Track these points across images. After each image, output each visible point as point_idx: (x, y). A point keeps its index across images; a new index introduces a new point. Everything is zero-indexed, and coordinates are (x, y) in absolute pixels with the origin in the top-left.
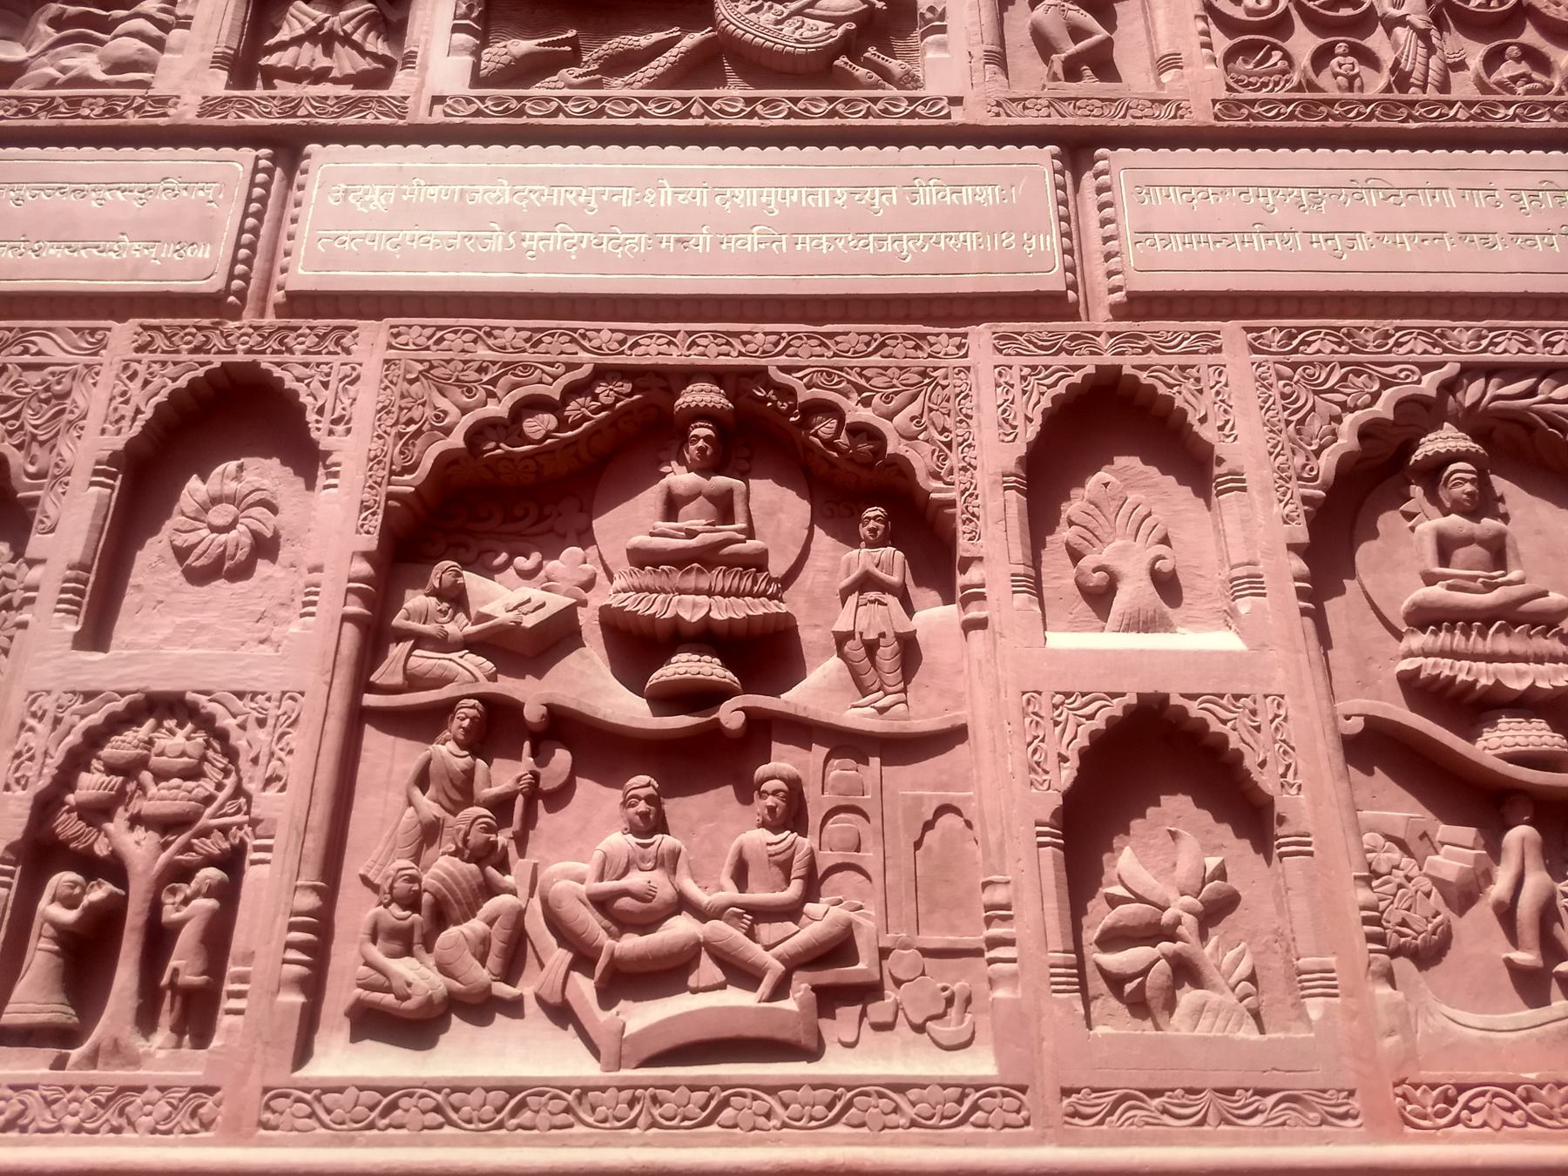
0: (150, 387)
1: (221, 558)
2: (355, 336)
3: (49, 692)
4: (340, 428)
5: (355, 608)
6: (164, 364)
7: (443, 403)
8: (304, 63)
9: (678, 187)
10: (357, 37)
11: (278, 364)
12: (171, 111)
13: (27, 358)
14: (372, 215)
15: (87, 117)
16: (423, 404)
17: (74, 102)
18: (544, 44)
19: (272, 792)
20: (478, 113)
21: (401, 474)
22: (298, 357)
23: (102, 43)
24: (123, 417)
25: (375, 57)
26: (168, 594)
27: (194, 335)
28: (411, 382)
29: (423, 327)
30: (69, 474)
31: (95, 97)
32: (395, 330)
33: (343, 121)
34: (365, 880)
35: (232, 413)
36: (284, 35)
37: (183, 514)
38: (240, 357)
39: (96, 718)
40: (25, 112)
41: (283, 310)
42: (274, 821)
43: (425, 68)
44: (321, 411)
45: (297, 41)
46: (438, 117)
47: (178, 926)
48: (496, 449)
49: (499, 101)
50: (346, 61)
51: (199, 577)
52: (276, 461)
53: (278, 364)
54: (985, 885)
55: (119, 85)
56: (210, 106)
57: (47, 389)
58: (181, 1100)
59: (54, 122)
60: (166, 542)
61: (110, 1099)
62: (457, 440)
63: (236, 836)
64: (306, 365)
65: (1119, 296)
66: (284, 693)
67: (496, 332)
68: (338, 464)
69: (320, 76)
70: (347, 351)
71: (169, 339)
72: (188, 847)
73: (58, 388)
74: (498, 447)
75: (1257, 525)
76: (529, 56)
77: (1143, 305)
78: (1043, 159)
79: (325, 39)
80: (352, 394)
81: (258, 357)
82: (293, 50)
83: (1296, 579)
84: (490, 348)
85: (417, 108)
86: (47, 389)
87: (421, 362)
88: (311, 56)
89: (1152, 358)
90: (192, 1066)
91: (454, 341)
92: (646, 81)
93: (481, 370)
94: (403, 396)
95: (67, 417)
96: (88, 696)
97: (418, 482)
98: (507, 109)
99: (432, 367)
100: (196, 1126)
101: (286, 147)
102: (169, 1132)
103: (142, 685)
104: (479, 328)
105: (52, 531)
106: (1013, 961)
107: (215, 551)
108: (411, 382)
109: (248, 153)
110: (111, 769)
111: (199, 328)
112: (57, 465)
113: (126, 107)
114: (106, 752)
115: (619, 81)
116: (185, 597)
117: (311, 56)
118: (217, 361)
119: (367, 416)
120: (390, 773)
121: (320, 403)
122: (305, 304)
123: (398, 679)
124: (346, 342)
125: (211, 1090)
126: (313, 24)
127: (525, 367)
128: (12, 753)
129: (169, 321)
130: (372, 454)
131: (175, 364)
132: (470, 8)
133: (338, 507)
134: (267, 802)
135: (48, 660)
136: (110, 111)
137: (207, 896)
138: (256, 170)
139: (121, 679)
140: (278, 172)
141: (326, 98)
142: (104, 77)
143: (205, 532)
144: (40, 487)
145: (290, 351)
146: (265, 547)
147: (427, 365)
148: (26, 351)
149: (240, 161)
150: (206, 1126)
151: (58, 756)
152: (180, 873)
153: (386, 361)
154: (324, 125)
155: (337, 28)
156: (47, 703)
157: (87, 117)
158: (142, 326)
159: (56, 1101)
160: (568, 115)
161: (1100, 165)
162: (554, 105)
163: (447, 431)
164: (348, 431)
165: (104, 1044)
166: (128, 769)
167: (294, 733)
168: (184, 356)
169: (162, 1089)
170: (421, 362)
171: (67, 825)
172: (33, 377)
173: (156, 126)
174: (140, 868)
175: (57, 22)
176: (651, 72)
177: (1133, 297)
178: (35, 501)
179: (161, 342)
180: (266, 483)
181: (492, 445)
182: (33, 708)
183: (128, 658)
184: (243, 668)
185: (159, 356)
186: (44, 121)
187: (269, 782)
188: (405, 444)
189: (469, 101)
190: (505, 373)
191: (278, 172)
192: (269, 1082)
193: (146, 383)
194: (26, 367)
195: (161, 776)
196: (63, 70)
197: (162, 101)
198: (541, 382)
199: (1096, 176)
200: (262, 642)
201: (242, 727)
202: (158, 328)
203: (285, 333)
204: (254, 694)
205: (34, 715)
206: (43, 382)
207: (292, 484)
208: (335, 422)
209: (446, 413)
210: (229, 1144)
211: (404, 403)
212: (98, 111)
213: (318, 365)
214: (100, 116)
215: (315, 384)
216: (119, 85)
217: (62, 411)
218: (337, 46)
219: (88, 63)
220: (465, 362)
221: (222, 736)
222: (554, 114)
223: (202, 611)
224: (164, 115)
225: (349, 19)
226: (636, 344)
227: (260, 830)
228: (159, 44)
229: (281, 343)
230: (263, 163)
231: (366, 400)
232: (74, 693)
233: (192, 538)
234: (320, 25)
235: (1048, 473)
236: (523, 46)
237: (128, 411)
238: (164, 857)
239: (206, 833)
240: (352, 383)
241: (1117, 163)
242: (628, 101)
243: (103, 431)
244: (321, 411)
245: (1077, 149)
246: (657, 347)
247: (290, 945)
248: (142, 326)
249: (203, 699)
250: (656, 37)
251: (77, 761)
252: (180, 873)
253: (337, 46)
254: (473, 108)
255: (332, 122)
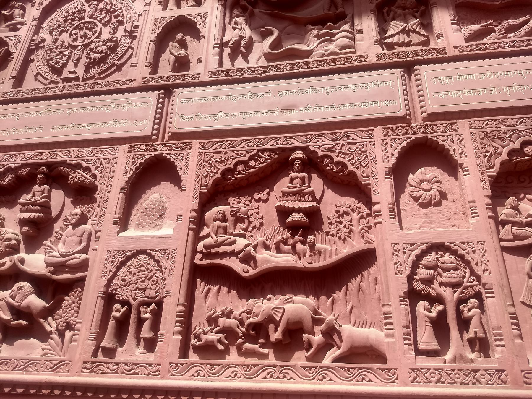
0: (393, 147)
1: (431, 200)
2: (457, 126)
3: (398, 244)
4: (463, 155)
5: (192, 226)
6: (395, 139)
7: (496, 145)
8: (401, 40)
9: (495, 73)
10: (417, 30)
11: (434, 137)
12: (367, 60)
13: (349, 141)
14: (191, 110)
15: (340, 65)
16: (489, 146)
17: (334, 60)
18: (483, 26)
19: (486, 274)
20: (471, 50)
21: (489, 169)
22: (440, 134)
23: (334, 41)
24: (388, 157)
25: (424, 35)
26: (416, 212)
27: (402, 130)
28: (482, 139)
29: (479, 121)
30: (377, 176)
31: (340, 58)
32: (470, 123)
33: (426, 57)
34: (523, 303)
35: (155, 171)
36: (389, 34)
37: (411, 186)
38: (420, 135)
39: (418, 251)
40: (319, 65)
41: (171, 138)
42: (492, 284)
43: (447, 38)
44: (454, 150)
45: (398, 34)
46: (456, 53)
47: (471, 318)
48: (517, 159)
49: (477, 46)
50: (415, 38)
51: (424, 206)
52: (435, 168)
53: (434, 137)
54: (383, 305)
55: (346, 53)
56: (379, 57)
57: (360, 150)
58: (493, 374)
59: (330, 67)
60: (408, 195)
61: (469, 373)
62: (219, 175)
63: (477, 289)
64: (444, 136)
65: (425, 115)
66: (478, 242)
67: (505, 120)
68: (467, 167)
69: (408, 44)
70: (456, 131)
71: (394, 131)
72: (462, 293)
73: (363, 149)
74: (517, 158)
75: (472, 185)
76: (479, 30)
77: (434, 117)
78: (399, 71)
79: (407, 32)
80: (463, 144)
81: (427, 135)
82: (396, 37)
83: (486, 205)
84: (505, 126)
85: (450, 51)
86: (360, 150)
87: (483, 132)
88: (403, 38)
89: (173, 152)
90: (150, 357)
91: (493, 124)
92: (522, 34)
93: (505, 133)
94: (481, 144)
95: (369, 158)
96: (412, 244)
97: (497, 171)
98: (481, 48)
99: (488, 133)
100: (500, 382)
101: (168, 90)
102: (493, 384)
103: (429, 241)
104: (499, 120)
105: (378, 193)
106: (392, 329)
107: (428, 198)
108: (482, 139)
109: (156, 92)
110: (427, 268)
111: (403, 127)
112: (372, 173)
113: (352, 60)
114: (423, 262)
115: (511, 35)
116: (422, 212)
117: (403, 38)
118: (413, 137)
119: (194, 167)
120: (517, 268)
121: (453, 148)
122: (176, 136)
123: (511, 237)
124: (455, 127)
125: (503, 371)
126: (402, 28)
127: (520, 131)
128: (393, 263)
129: (392, 126)
130: (478, 163)
131: (399, 139)
132: (455, 17)
133: (473, 181)
134: (485, 277)
135: (394, 233)
136: (347, 62)
137: (476, 308)
138: (159, 98)
139: (421, 239)
140: (166, 99)
141: (417, 50)
142: (340, 51)
143: (422, 191)
144: (369, 180)
145: (437, 132)
146: (443, 195)
147: (486, 133)
148: (348, 139)
149: (153, 97)
150: (505, 383)
151: (410, 264)
152: (462, 301)
153: (471, 133)
154: (420, 59)
155: (410, 28)
156: (399, 247)
157: (340, 65)
158: (383, 128)
159: (451, 374)
160: (502, 48)
161: (417, 72)
162: (497, 45)
163: (500, 154)
164: (466, 156)
165: (457, 356)
166: (434, 267)
167: (487, 255)
168: (401, 137)
169: (485, 371)
170: (483, 132)
171: (418, 286)
172: (354, 147)
173: (333, 68)
174: (449, 299)
175: (318, 37)
176: (524, 31)
177: (430, 115)
178: (369, 184)
179: (391, 133)
180: (436, 175)
181: (515, 158)
182: (395, 248)
183: (421, 232)
184: (461, 234)
185: (392, 137)
186: (326, 67)
187: (485, 270)
188: (488, 159)
189: (467, 47)
190: (513, 134)
191: (166, 99)
192: (523, 369)
193: (392, 146)
194: (350, 144)
195: (445, 270)
196: (326, 51)
197: (363, 57)
198: (527, 136)
199: (416, 75)
200: (453, 226)
201: (468, 253)
202: (389, 128)
203: (433, 126)
204: (468, 243)
205: (396, 251)
206: (357, 148)
207: (443, 175)
208: (461, 153)
209: (498, 148)
210: (515, 389)
211: (482, 146)
212: (343, 62)
213: (448, 136)
214: (344, 64)
215: (449, 142)
216: (346, 53)
217: (367, 156)
218: (411, 34)
219: (332, 47)
220: (498, 131)
221: (462, 257)
222: (498, 48)
223: (429, 217)
224: (365, 61)
225: (414, 25)
226: (521, 122)
227: (486, 286)
228: (353, 39)
229: (432, 129)
230: (161, 95)
231: (193, 165)
232: (407, 244)
233: (419, 194)
234: (405, 28)
235: (399, 173)
236: (478, 27)
237: (389, 154)
238: (456, 295)
239: (466, 288)
240: (462, 140)
241: (423, 70)
242: (523, 41)
243: (383, 162)
244: (454, 150)
245: (408, 68)
246: (282, 142)
247: (177, 322)
248: (383, 128)
249: (452, 245)
250: (522, 19)
251: (415, 265)
252: (462, 301)
253: (411, 34)
254: (469, 49)
255: (422, 58)
